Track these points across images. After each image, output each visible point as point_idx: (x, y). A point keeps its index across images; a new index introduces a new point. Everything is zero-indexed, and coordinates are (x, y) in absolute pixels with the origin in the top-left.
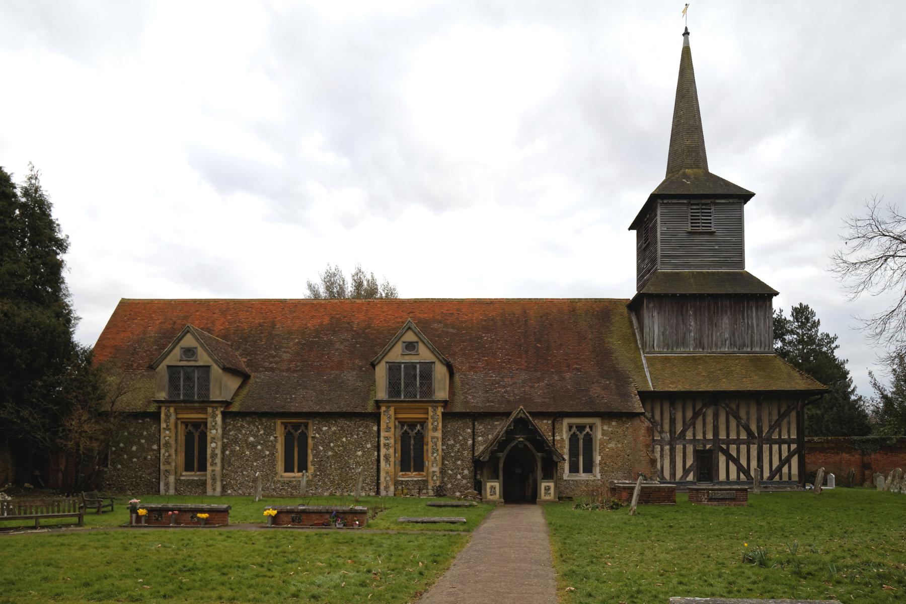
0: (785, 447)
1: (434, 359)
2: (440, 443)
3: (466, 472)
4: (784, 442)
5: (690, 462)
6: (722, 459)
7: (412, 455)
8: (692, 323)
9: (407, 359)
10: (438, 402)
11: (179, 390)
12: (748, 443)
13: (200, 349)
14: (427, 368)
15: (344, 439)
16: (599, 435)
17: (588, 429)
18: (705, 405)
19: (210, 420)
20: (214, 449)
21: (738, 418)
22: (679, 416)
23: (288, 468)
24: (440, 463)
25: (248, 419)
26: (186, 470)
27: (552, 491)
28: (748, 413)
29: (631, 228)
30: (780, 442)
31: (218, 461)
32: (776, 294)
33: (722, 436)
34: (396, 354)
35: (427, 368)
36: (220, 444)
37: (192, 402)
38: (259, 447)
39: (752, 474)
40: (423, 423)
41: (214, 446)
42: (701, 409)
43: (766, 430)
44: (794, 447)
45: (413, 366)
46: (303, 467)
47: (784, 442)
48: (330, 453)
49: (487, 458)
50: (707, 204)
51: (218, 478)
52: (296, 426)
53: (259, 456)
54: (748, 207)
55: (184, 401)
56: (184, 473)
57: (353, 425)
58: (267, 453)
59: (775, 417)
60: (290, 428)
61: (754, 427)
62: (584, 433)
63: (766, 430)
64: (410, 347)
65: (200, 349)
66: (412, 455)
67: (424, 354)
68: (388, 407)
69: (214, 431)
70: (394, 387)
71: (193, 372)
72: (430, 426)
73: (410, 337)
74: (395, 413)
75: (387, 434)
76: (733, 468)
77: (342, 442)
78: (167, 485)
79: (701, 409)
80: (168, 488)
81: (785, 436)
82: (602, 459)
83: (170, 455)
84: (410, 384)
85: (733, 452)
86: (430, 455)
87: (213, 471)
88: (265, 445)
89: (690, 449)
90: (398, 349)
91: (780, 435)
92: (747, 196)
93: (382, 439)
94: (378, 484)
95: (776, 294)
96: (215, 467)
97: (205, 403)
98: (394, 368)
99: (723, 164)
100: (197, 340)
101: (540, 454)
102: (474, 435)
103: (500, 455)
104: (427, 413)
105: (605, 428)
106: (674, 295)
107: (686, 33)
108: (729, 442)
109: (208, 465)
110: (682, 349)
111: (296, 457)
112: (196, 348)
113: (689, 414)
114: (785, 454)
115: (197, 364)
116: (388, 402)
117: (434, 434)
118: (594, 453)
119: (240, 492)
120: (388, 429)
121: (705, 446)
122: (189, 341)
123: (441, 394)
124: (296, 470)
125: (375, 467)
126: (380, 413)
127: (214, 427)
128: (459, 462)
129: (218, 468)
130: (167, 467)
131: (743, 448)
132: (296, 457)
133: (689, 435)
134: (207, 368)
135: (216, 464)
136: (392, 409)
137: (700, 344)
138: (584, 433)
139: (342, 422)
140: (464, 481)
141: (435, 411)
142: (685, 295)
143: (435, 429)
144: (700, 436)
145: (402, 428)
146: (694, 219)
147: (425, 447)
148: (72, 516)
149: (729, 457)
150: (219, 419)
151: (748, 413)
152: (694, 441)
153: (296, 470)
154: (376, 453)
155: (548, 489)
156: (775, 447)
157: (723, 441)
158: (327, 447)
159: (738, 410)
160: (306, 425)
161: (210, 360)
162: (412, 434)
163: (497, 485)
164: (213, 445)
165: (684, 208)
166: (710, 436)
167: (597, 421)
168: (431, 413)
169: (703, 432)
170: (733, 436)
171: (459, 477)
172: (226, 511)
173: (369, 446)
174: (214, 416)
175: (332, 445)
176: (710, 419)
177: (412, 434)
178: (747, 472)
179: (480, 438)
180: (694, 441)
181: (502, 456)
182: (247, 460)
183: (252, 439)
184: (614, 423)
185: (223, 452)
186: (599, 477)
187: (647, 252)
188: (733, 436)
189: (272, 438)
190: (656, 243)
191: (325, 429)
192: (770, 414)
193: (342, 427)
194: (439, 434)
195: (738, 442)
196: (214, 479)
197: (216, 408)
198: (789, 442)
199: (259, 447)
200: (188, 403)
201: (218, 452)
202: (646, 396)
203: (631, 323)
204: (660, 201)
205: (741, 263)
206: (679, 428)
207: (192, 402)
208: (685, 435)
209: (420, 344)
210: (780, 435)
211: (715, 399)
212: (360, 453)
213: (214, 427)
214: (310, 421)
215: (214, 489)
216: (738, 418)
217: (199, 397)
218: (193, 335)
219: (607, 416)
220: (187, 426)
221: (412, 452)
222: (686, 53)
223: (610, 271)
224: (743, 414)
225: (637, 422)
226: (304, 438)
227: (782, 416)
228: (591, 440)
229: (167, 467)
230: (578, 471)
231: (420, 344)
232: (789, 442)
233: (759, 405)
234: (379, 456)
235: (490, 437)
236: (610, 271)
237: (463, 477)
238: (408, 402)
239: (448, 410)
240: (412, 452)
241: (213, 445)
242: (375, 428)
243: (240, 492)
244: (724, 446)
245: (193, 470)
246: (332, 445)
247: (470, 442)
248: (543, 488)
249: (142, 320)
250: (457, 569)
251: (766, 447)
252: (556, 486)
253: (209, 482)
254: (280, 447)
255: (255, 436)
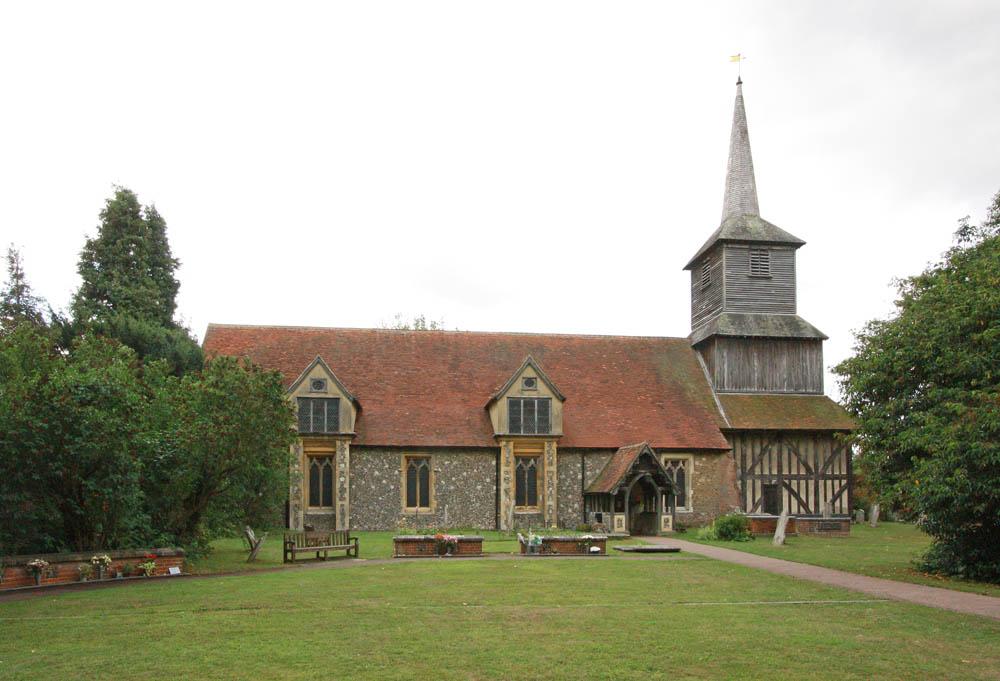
0: (837, 482)
1: (551, 395)
2: (555, 478)
3: (576, 505)
4: (836, 477)
5: (758, 496)
6: (785, 493)
7: (526, 492)
8: (756, 364)
9: (527, 395)
10: (552, 437)
11: (309, 422)
12: (807, 479)
13: (330, 382)
14: (544, 404)
15: (465, 474)
16: (692, 471)
17: (681, 464)
18: (770, 443)
19: (338, 453)
20: (342, 484)
21: (797, 454)
22: (749, 452)
23: (411, 503)
24: (555, 496)
25: (373, 452)
26: (311, 504)
27: (670, 523)
28: (806, 451)
29: (687, 268)
30: (833, 478)
31: (347, 495)
32: (826, 338)
33: (785, 472)
34: (517, 390)
35: (544, 404)
36: (348, 478)
37: (323, 435)
38: (384, 481)
39: (812, 508)
40: (332, 457)
41: (341, 481)
42: (767, 446)
43: (821, 466)
44: (844, 482)
45: (529, 403)
46: (425, 503)
47: (836, 477)
48: (452, 488)
49: (616, 492)
50: (764, 250)
51: (347, 512)
52: (417, 457)
53: (384, 490)
54: (799, 252)
55: (315, 434)
56: (310, 508)
57: (472, 459)
58: (392, 487)
59: (829, 454)
60: (412, 461)
61: (811, 464)
62: (678, 468)
63: (821, 466)
64: (530, 382)
65: (330, 382)
66: (526, 492)
67: (542, 390)
68: (508, 442)
69: (343, 465)
70: (514, 424)
71: (323, 404)
72: (546, 461)
73: (530, 373)
74: (514, 447)
75: (507, 468)
76: (794, 502)
77: (463, 476)
78: (296, 519)
79: (767, 446)
80: (298, 524)
81: (837, 473)
82: (694, 493)
83: (299, 490)
84: (528, 416)
85: (795, 488)
86: (546, 489)
87: (342, 505)
88: (390, 479)
89: (758, 484)
90: (519, 385)
91: (833, 471)
92: (798, 244)
93: (502, 473)
94: (497, 519)
95: (826, 338)
96: (342, 503)
97: (335, 436)
98: (514, 403)
99: (777, 212)
100: (328, 371)
101: (660, 488)
102: (583, 468)
103: (626, 488)
104: (543, 448)
105: (697, 463)
106: (741, 337)
107: (740, 83)
108: (791, 477)
109: (337, 499)
110: (748, 389)
111: (418, 492)
112: (325, 380)
113: (758, 451)
114: (837, 490)
115: (327, 396)
116: (509, 436)
117: (549, 468)
118: (687, 488)
119: (366, 527)
120: (508, 464)
121: (771, 481)
122: (319, 372)
123: (557, 430)
124: (418, 504)
125: (494, 501)
126: (500, 448)
127: (343, 461)
128: (570, 496)
129: (346, 503)
130: (297, 502)
131: (803, 482)
132: (418, 492)
133: (757, 471)
134: (336, 401)
135: (345, 498)
136: (512, 443)
137: (762, 384)
138: (678, 468)
139: (464, 457)
140: (575, 515)
141: (550, 446)
142: (751, 337)
143: (551, 464)
144: (766, 472)
145: (311, 461)
146: (754, 264)
147: (539, 482)
148: (340, 548)
149: (791, 491)
150: (347, 453)
151: (806, 451)
152: (762, 476)
153: (418, 504)
154: (495, 488)
155: (667, 521)
156: (829, 482)
157: (786, 477)
158: (448, 480)
159: (798, 447)
160: (428, 459)
161: (338, 391)
162: (526, 468)
163: (622, 517)
164: (342, 479)
165: (746, 253)
166: (775, 472)
167: (690, 458)
168: (546, 449)
169: (770, 469)
170: (794, 472)
171: (570, 510)
172: (480, 541)
173: (488, 480)
174: (343, 450)
175: (453, 479)
176: (775, 455)
177: (526, 468)
178: (806, 506)
179: (588, 473)
180: (762, 476)
181: (628, 490)
182: (373, 495)
183: (377, 473)
184: (704, 459)
185: (350, 485)
186: (691, 510)
187: (707, 293)
188: (794, 472)
189: (396, 472)
190: (722, 284)
191: (446, 463)
192: (825, 452)
193: (463, 461)
194: (554, 468)
195: (798, 477)
196: (343, 514)
197: (345, 441)
198: (840, 478)
199: (384, 481)
200: (317, 436)
201: (347, 486)
202: (727, 433)
203: (698, 364)
204: (725, 246)
205: (793, 308)
206: (749, 464)
207: (323, 435)
208: (754, 471)
209: (539, 380)
210: (833, 471)
211: (779, 436)
212: (479, 487)
213: (343, 461)
214: (433, 456)
215: (343, 524)
216: (797, 454)
217: (314, 428)
218: (323, 366)
219: (698, 452)
220: (311, 460)
221: (526, 486)
222: (740, 99)
223: (665, 311)
224: (802, 450)
225: (724, 457)
226: (426, 472)
227: (834, 454)
228: (683, 475)
229: (297, 502)
230: (415, 505)
231: (539, 380)
232: (840, 478)
233: (816, 442)
234: (498, 490)
235: (598, 471)
236: (665, 311)
237: (574, 511)
238: (526, 436)
239: (562, 446)
240: (526, 486)
241: (342, 479)
242: (494, 463)
243: (366, 527)
244: (787, 481)
245: (318, 505)
246: (453, 479)
247: (580, 477)
248: (663, 520)
249: (236, 347)
250: (986, 598)
251: (821, 482)
252: (674, 518)
253: (338, 517)
254: (404, 480)
255: (380, 470)
